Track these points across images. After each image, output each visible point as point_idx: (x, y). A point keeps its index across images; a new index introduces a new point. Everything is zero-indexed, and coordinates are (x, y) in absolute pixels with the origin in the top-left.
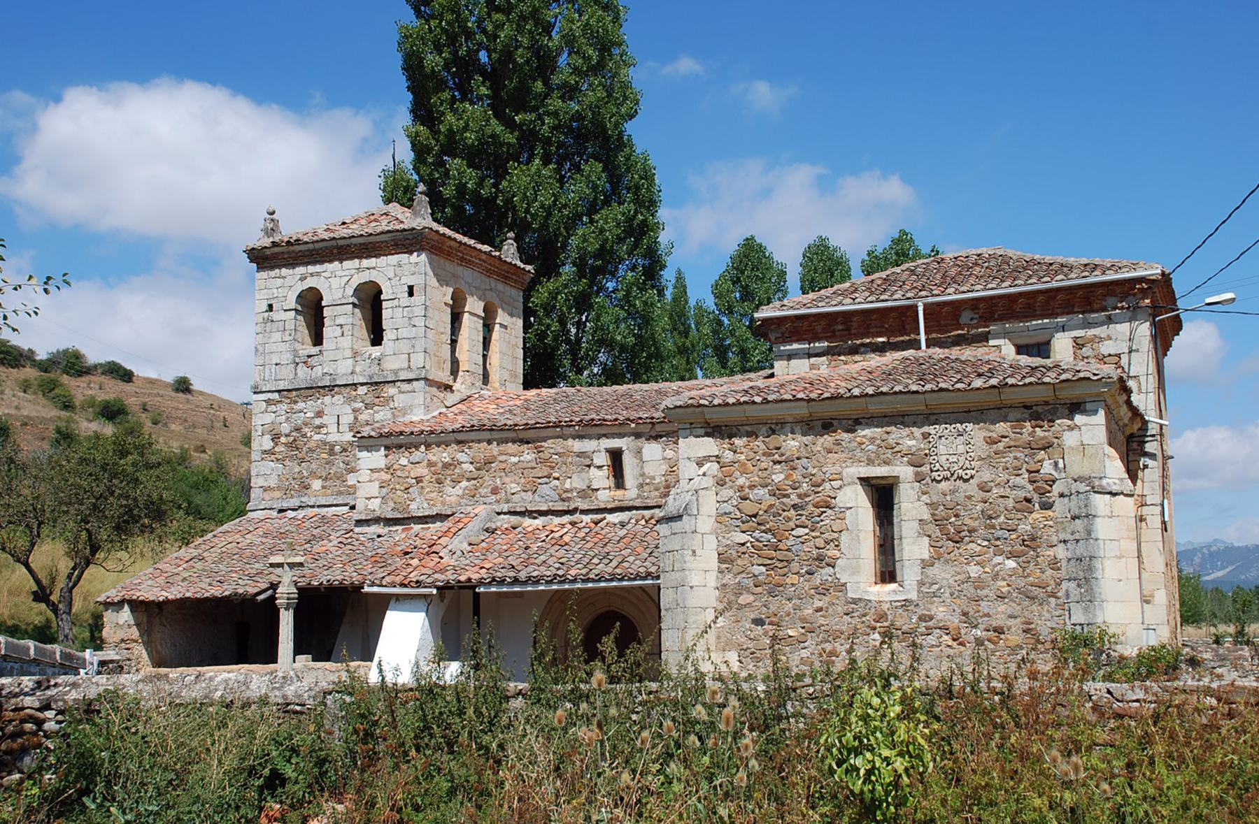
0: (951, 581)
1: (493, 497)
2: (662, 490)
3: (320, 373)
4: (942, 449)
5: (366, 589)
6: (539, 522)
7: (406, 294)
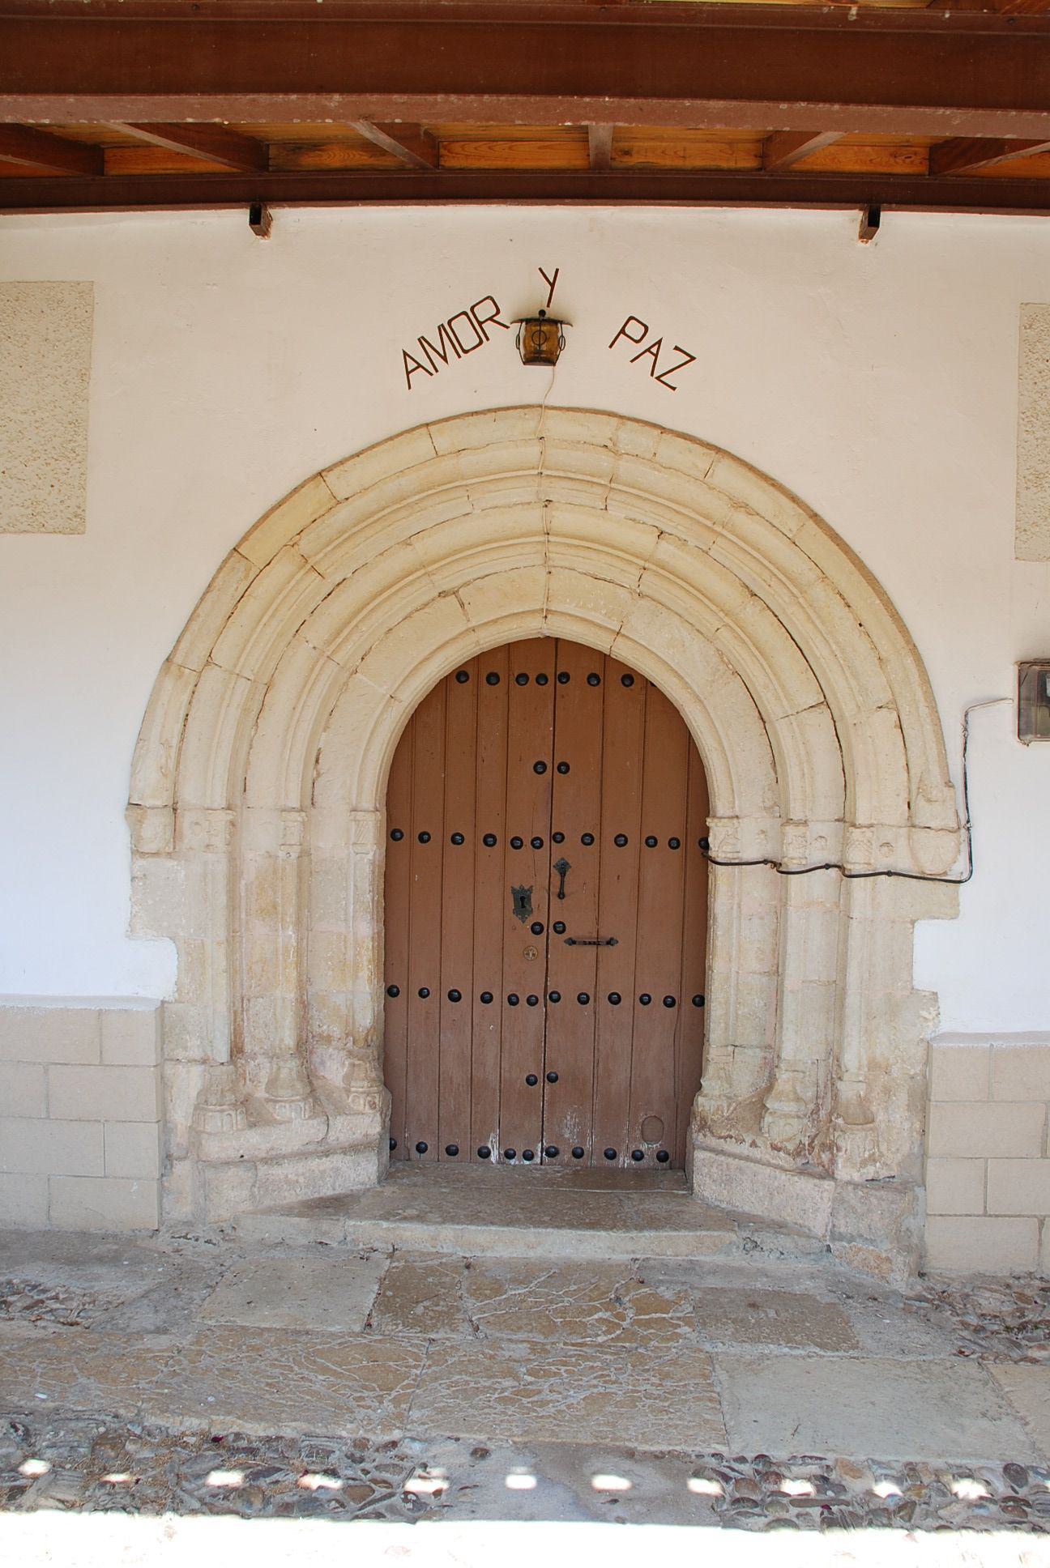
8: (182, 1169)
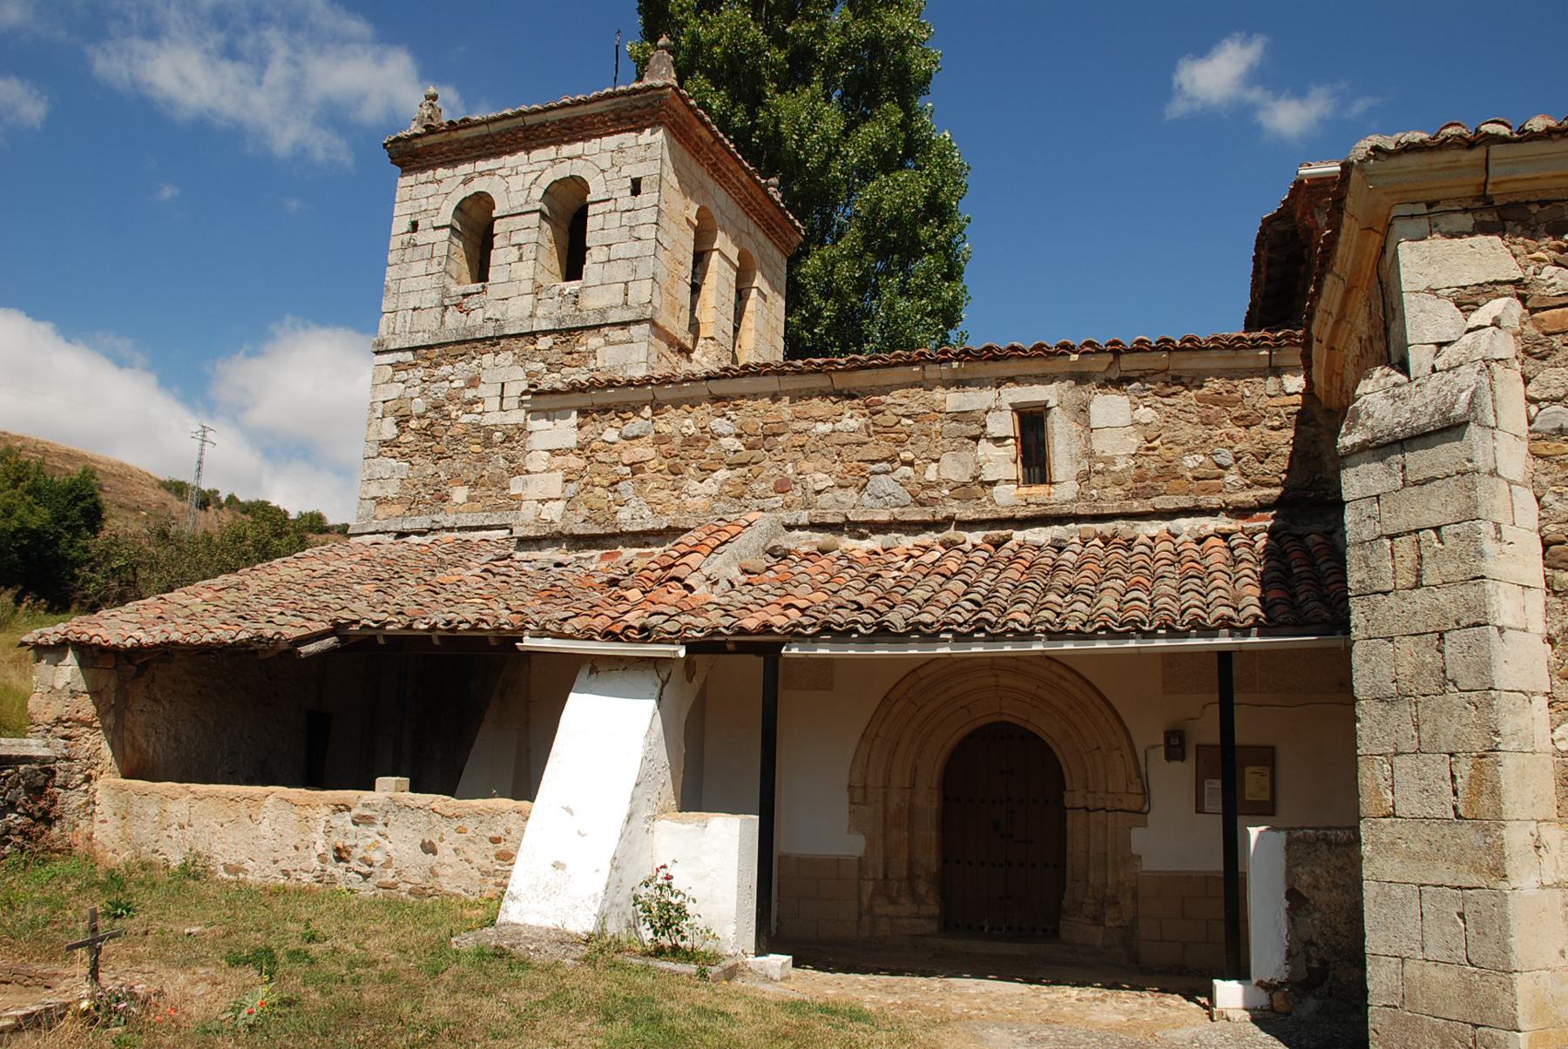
1: (779, 498)
2: (1130, 484)
3: (479, 321)
5: (528, 642)
6: (875, 542)
7: (628, 192)
8: (866, 919)
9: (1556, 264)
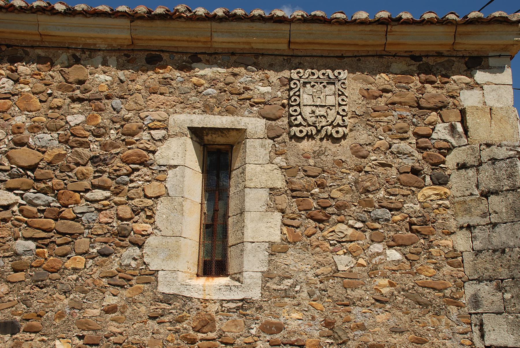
0: (310, 275)
4: (306, 99)
9: (8, 77)
